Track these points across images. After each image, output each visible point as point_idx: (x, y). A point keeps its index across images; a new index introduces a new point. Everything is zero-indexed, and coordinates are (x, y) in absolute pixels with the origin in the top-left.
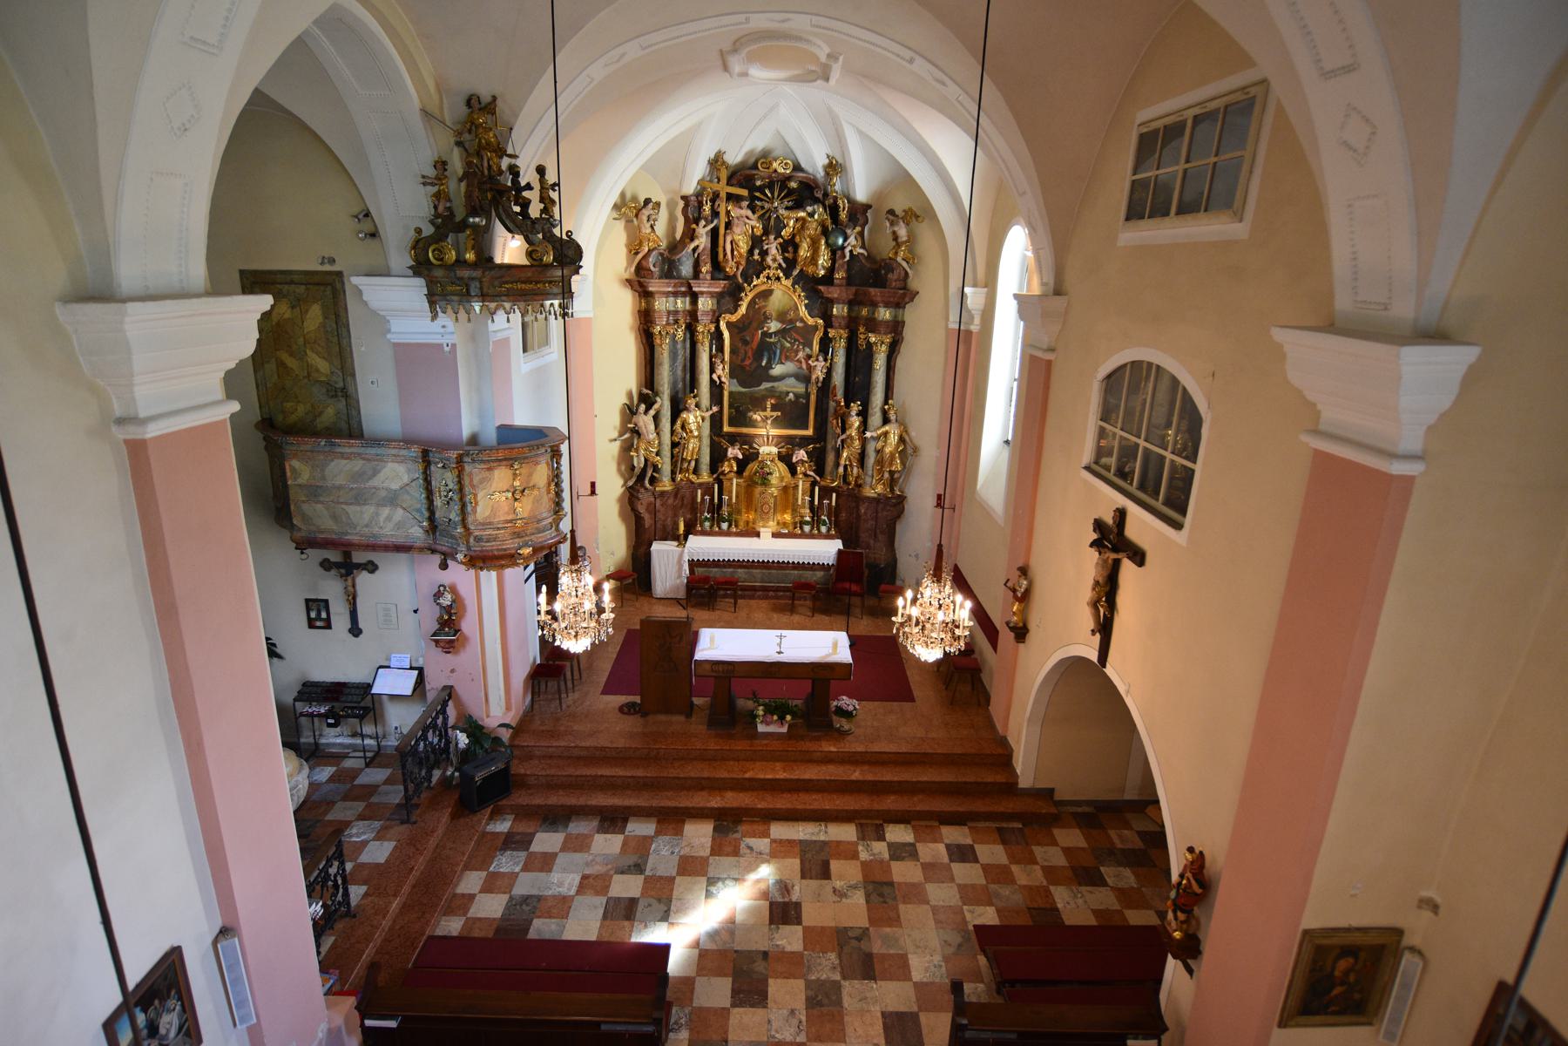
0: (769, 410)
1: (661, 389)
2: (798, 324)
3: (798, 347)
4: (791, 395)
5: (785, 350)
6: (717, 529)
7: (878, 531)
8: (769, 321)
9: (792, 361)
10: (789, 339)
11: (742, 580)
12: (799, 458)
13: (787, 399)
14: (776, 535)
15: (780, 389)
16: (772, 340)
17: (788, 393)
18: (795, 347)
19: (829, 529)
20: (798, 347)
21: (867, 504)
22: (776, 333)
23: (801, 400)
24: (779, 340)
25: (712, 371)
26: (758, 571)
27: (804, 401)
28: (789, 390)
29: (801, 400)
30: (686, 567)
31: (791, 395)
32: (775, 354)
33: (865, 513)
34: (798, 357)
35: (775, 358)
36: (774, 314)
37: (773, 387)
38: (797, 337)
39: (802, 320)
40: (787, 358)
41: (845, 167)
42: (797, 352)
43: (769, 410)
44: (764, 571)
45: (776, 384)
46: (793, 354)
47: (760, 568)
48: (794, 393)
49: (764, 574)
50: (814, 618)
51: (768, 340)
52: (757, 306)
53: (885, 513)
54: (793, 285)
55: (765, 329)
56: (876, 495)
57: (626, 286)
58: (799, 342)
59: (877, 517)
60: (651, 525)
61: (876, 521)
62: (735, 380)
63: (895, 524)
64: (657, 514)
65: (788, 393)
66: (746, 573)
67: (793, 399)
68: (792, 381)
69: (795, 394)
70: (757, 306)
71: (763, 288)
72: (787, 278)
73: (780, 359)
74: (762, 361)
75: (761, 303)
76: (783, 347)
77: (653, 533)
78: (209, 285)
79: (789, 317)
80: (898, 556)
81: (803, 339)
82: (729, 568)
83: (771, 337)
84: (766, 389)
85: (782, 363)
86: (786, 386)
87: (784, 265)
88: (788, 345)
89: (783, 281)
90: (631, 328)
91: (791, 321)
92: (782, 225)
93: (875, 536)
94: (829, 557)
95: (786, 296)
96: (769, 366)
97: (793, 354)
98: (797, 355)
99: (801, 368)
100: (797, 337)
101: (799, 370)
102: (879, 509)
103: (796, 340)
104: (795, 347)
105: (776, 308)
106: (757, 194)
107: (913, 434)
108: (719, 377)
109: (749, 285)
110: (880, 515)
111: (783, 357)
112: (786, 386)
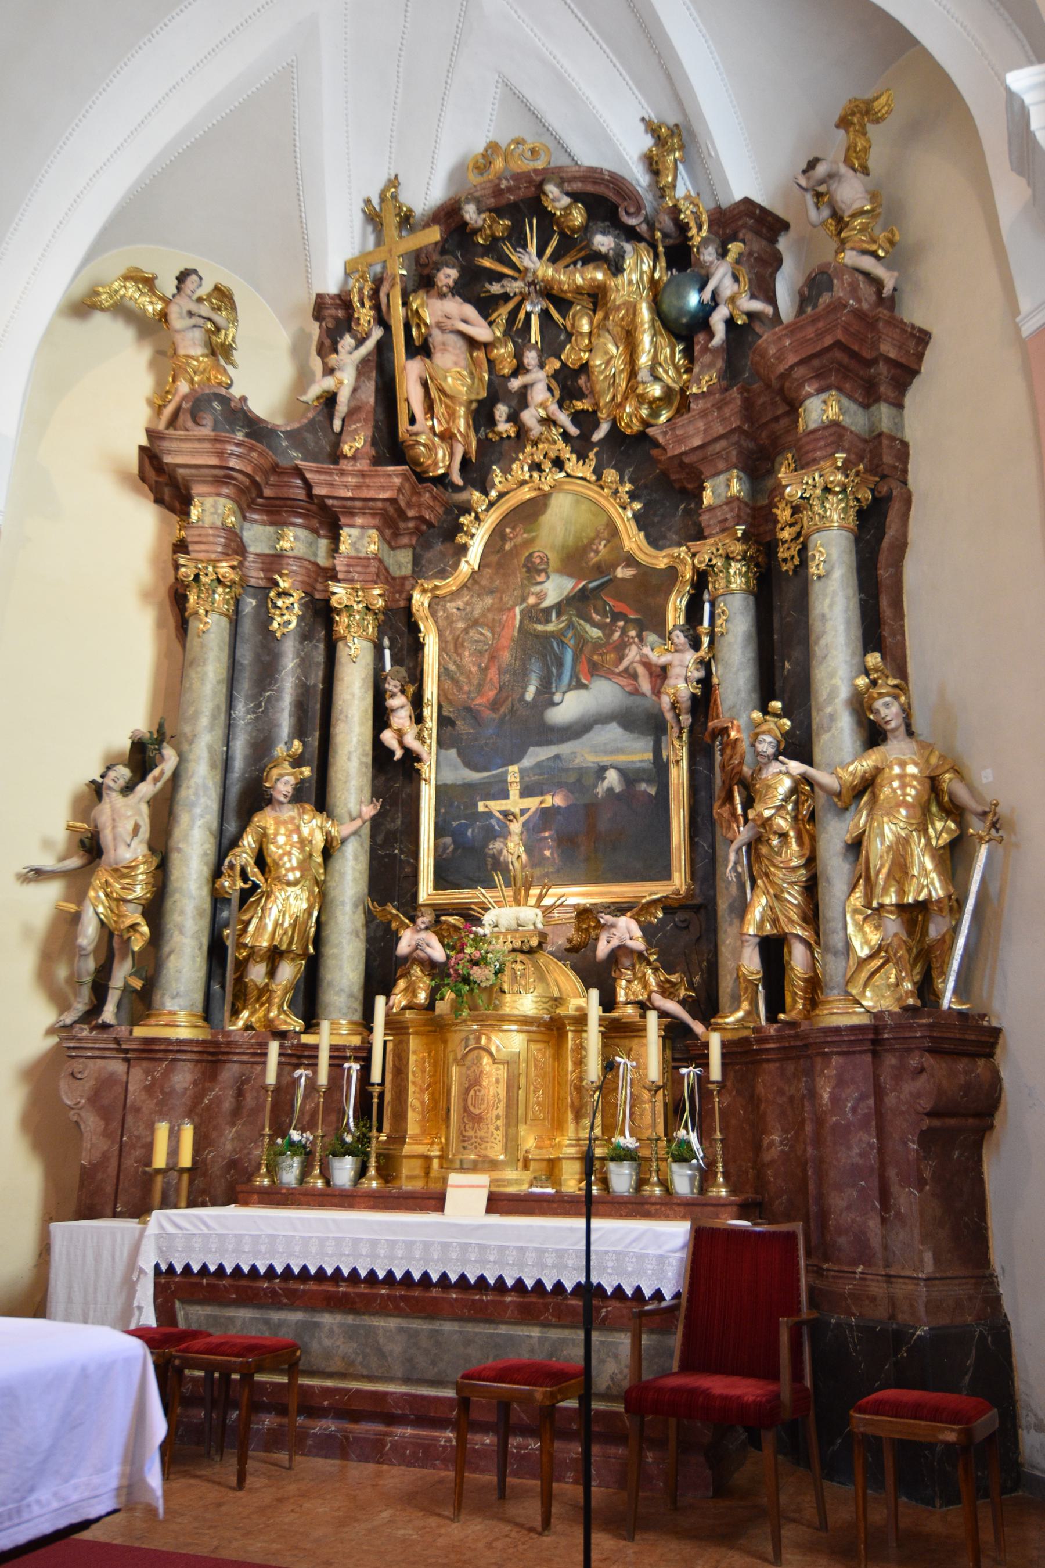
0: (514, 791)
1: (187, 729)
2: (621, 573)
3: (624, 632)
4: (612, 777)
5: (587, 650)
6: (320, 1184)
7: (892, 1173)
8: (541, 578)
9: (609, 675)
10: (597, 618)
11: (336, 1365)
12: (615, 943)
13: (601, 789)
14: (497, 1203)
15: (578, 762)
16: (550, 627)
17: (602, 770)
18: (617, 635)
19: (706, 1177)
20: (624, 632)
21: (835, 1060)
22: (559, 608)
23: (643, 786)
24: (570, 625)
25: (381, 717)
26: (392, 1323)
27: (652, 791)
28: (605, 760)
29: (643, 786)
30: (145, 1293)
31: (612, 777)
32: (560, 664)
33: (834, 1099)
34: (625, 663)
35: (560, 676)
36: (554, 558)
37: (557, 757)
38: (620, 607)
39: (630, 560)
40: (595, 670)
41: (692, 133)
42: (621, 649)
43: (514, 791)
44: (416, 1324)
45: (564, 749)
46: (611, 657)
47: (399, 1313)
48: (620, 770)
49: (414, 1334)
50: (547, 1540)
51: (540, 627)
52: (508, 546)
53: (909, 1087)
54: (598, 472)
55: (532, 600)
56: (865, 1020)
57: (137, 490)
58: (627, 621)
59: (879, 1112)
60: (105, 1156)
61: (881, 1134)
62: (453, 753)
63: (979, 1161)
64: (130, 1119)
65: (602, 770)
66: (351, 1333)
67: (618, 789)
68: (613, 732)
69: (622, 772)
70: (508, 546)
71: (526, 494)
72: (582, 456)
73: (575, 675)
74: (524, 689)
75: (517, 536)
76: (581, 641)
77: (109, 1189)
78: (93, 998)
79: (593, 558)
80: (1008, 1306)
81: (637, 611)
82: (292, 1307)
83: (548, 621)
84: (539, 765)
85: (581, 686)
86: (595, 750)
87: (574, 431)
88: (595, 633)
89: (572, 464)
90: (146, 596)
91: (600, 569)
92: (562, 337)
93: (885, 1195)
94: (661, 1259)
95: (584, 506)
96: (546, 698)
97: (611, 657)
98: (621, 659)
99: (636, 692)
100: (620, 607)
101: (630, 701)
102: (886, 1079)
103: (616, 616)
104: (617, 635)
105: (559, 540)
106: (487, 263)
107: (985, 777)
108: (400, 734)
109: (486, 493)
110: (890, 1100)
111: (584, 666)
112: (595, 750)
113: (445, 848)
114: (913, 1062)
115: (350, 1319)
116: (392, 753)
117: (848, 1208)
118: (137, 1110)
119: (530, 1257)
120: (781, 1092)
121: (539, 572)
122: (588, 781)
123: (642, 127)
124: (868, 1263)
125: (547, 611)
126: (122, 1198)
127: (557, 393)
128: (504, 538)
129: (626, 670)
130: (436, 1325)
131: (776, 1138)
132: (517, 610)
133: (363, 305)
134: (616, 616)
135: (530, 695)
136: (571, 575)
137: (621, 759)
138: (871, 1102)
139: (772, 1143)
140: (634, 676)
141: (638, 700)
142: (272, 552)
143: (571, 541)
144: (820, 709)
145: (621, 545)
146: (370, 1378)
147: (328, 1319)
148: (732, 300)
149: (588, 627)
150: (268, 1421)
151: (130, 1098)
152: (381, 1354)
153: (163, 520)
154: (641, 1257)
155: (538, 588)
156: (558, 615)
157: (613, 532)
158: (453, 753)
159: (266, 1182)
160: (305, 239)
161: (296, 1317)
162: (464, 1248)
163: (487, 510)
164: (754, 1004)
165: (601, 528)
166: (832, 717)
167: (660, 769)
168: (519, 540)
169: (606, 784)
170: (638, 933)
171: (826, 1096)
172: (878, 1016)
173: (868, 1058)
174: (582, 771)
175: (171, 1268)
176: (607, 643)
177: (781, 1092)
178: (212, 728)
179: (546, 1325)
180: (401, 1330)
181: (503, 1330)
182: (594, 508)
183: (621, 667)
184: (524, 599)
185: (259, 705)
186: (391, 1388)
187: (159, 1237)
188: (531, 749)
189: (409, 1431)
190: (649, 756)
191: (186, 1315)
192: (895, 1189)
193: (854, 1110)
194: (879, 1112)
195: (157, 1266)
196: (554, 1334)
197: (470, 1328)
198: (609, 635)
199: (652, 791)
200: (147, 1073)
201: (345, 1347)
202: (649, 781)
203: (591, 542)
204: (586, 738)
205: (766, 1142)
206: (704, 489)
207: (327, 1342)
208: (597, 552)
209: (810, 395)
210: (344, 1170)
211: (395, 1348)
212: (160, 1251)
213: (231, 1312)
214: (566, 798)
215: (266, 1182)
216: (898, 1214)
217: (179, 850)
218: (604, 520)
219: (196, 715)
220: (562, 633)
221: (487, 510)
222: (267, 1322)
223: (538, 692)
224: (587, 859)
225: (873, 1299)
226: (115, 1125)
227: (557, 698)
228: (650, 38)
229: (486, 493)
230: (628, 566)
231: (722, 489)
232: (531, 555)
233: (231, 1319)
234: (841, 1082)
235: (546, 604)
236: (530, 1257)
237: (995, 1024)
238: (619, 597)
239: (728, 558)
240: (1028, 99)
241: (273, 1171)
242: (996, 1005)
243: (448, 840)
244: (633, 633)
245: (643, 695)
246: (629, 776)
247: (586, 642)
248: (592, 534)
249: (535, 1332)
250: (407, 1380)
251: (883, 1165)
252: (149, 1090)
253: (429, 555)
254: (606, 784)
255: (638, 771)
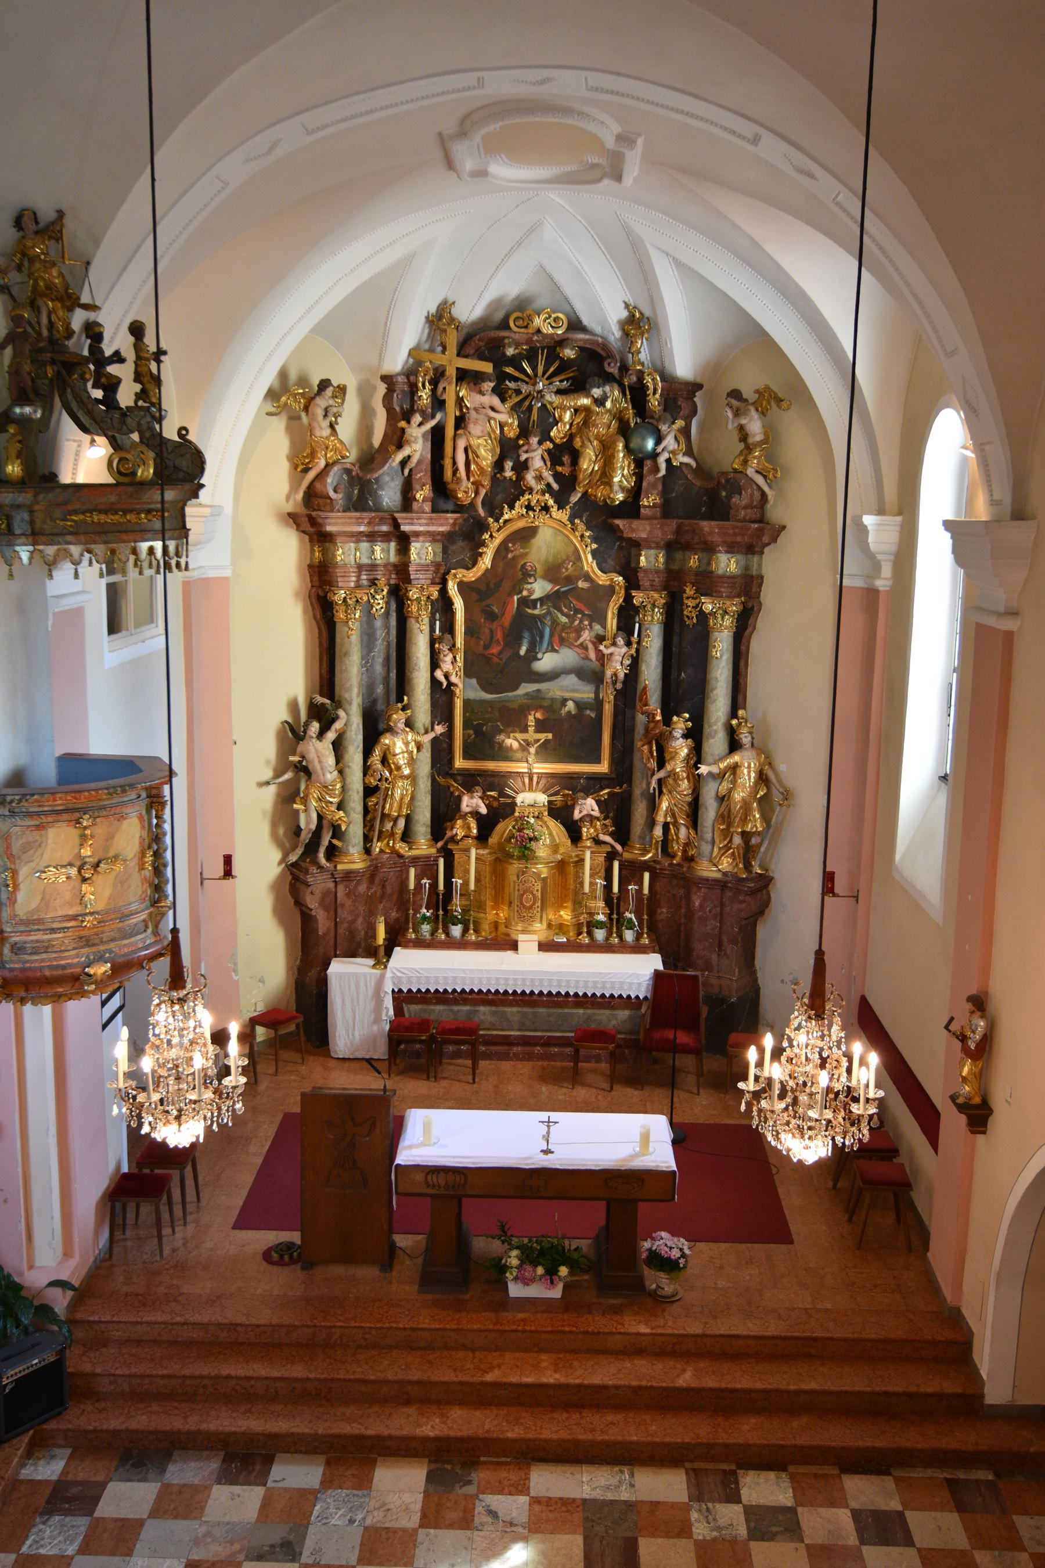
0: (531, 729)
1: (347, 696)
2: (581, 584)
3: (581, 621)
4: (570, 705)
5: (559, 628)
7: (725, 938)
8: (531, 580)
9: (571, 646)
11: (487, 1025)
12: (585, 812)
13: (564, 711)
14: (545, 947)
15: (551, 694)
16: (536, 612)
17: (564, 701)
18: (577, 622)
19: (639, 936)
20: (581, 621)
24: (549, 612)
25: (435, 664)
26: (515, 1009)
27: (593, 715)
28: (567, 695)
29: (588, 712)
30: (388, 1003)
31: (570, 705)
32: (542, 636)
33: (701, 906)
34: (581, 640)
35: (541, 641)
37: (539, 691)
38: (579, 605)
39: (587, 577)
40: (563, 642)
41: (656, 324)
42: (579, 631)
43: (531, 729)
44: (525, 1010)
45: (543, 686)
47: (518, 1005)
50: (613, 1093)
51: (529, 611)
52: (510, 556)
53: (736, 906)
54: (571, 520)
55: (525, 593)
56: (719, 876)
58: (584, 615)
59: (721, 913)
60: (329, 929)
64: (339, 910)
65: (564, 701)
66: (495, 1013)
68: (572, 680)
70: (510, 556)
71: (521, 524)
73: (550, 643)
75: (516, 550)
76: (555, 623)
77: (332, 943)
79: (565, 573)
80: (760, 982)
83: (535, 608)
84: (527, 694)
86: (562, 689)
87: (555, 486)
88: (564, 619)
90: (297, 594)
91: (569, 580)
93: (720, 946)
94: (639, 984)
96: (532, 655)
97: (573, 635)
98: (579, 637)
99: (587, 658)
100: (579, 605)
101: (583, 663)
103: (577, 611)
104: (577, 622)
106: (509, 370)
107: (782, 768)
109: (497, 520)
110: (727, 909)
111: (556, 639)
113: (469, 736)
114: (741, 898)
115: (494, 1008)
116: (441, 684)
117: (703, 949)
118: (343, 905)
119: (581, 984)
120: (669, 892)
121: (530, 576)
122: (556, 706)
123: (623, 305)
124: (710, 971)
125: (535, 601)
126: (339, 947)
127: (549, 463)
128: (508, 550)
129: (581, 644)
130: (536, 1010)
131: (664, 910)
132: (516, 598)
133: (424, 387)
134: (577, 611)
135: (523, 651)
136: (550, 581)
137: (577, 695)
138: (718, 909)
139: (662, 913)
140: (586, 649)
141: (588, 663)
142: (369, 562)
143: (551, 559)
144: (710, 726)
145: (583, 567)
146: (502, 1030)
147: (482, 1008)
148: (673, 452)
149: (559, 615)
150: (451, 1048)
151: (339, 900)
152: (509, 1021)
153: (301, 541)
154: (630, 984)
155: (529, 586)
156: (541, 605)
157: (579, 558)
158: (474, 681)
159: (413, 936)
160: (385, 335)
161: (467, 1008)
162: (550, 981)
163: (498, 530)
164: (657, 850)
165: (570, 554)
166: (716, 732)
167: (598, 705)
168: (517, 553)
169: (567, 709)
170: (596, 808)
171: (697, 904)
172: (725, 874)
173: (719, 891)
174: (553, 700)
175: (400, 991)
176: (570, 627)
177: (669, 892)
178: (358, 696)
179: (586, 1008)
180: (518, 1012)
181: (566, 1010)
182: (566, 540)
183: (579, 642)
184: (521, 592)
185: (368, 662)
186: (512, 1033)
187: (392, 978)
188: (523, 684)
189: (519, 1048)
190: (592, 695)
191: (409, 1010)
192: (725, 944)
193: (710, 911)
194: (721, 913)
195: (393, 991)
196: (589, 1011)
197: (551, 1010)
198: (572, 622)
199: (593, 715)
200: (346, 887)
201: (490, 1019)
202: (591, 710)
203: (564, 562)
204: (556, 681)
205: (659, 911)
206: (640, 555)
207: (482, 1018)
208: (567, 569)
209: (720, 551)
210: (456, 931)
211: (516, 1018)
212: (394, 983)
213: (432, 1007)
214: (543, 714)
215: (413, 936)
216: (726, 954)
217: (349, 767)
218: (571, 549)
219: (350, 689)
220: (544, 616)
221: (498, 530)
222: (451, 1010)
223: (528, 651)
224: (554, 749)
225: (713, 986)
226: (332, 913)
227: (539, 656)
228: (646, 280)
229: (497, 520)
230: (585, 580)
231: (652, 559)
232: (525, 564)
233: (433, 1010)
234: (705, 899)
235: (534, 597)
236: (581, 984)
237: (771, 874)
238: (578, 599)
239: (654, 606)
240: (869, 528)
241: (416, 930)
242: (772, 867)
243: (471, 732)
244: (586, 623)
245: (591, 660)
246: (580, 705)
247: (558, 624)
248: (564, 557)
249: (581, 1011)
250: (519, 1030)
251: (720, 933)
252: (348, 895)
253: (453, 548)
254: (567, 709)
255: (586, 703)
